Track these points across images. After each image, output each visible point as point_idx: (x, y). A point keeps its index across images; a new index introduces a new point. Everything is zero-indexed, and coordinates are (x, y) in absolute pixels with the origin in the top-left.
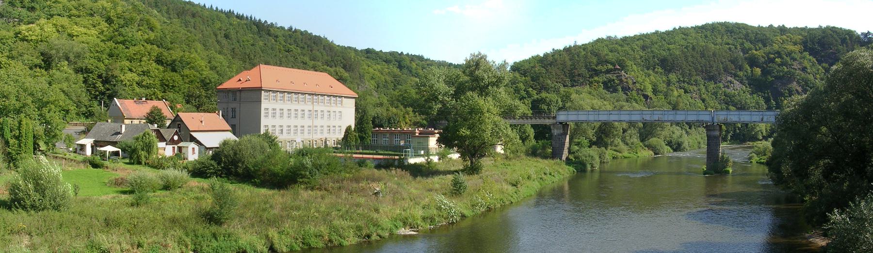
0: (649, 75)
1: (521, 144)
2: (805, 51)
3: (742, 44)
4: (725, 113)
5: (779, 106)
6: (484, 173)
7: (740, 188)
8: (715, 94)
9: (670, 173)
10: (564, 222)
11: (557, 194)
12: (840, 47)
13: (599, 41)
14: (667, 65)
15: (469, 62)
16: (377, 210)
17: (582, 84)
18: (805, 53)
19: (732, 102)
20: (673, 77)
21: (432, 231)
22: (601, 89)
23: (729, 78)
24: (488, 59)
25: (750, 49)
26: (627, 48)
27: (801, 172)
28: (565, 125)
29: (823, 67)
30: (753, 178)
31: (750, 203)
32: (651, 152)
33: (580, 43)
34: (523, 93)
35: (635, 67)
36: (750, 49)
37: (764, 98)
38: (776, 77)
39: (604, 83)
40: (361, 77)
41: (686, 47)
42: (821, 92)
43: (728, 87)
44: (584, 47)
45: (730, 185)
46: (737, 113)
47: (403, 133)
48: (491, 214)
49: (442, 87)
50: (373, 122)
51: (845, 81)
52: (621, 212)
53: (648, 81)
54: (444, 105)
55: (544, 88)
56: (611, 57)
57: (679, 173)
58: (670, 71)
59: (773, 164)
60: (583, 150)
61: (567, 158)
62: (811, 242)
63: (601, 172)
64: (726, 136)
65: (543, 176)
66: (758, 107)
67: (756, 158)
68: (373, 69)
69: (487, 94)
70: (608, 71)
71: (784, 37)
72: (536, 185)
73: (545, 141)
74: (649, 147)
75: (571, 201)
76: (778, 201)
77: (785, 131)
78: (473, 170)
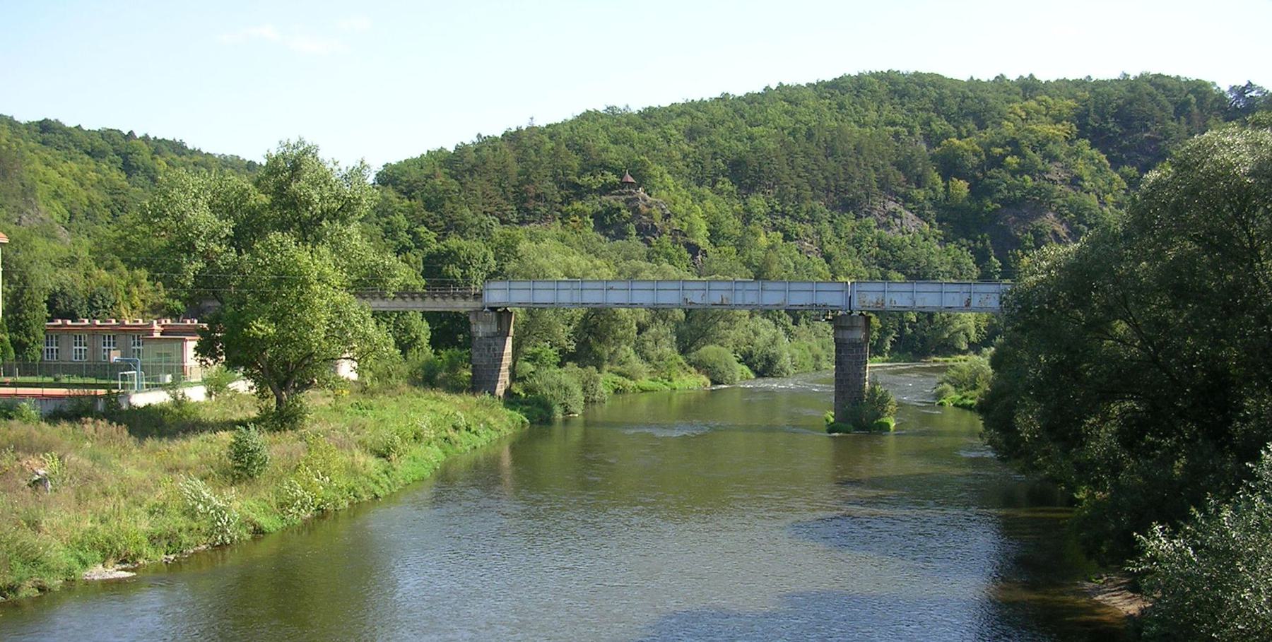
0: (702, 199)
1: (399, 358)
2: (1079, 136)
3: (927, 123)
4: (879, 287)
5: (1009, 272)
6: (310, 426)
7: (916, 467)
8: (856, 242)
9: (748, 428)
10: (502, 542)
11: (484, 475)
12: (1171, 125)
13: (588, 116)
14: (744, 175)
15: (276, 160)
16: (35, 525)
17: (544, 218)
18: (1080, 142)
19: (897, 260)
20: (758, 202)
21: (178, 563)
22: (589, 231)
23: (891, 206)
24: (320, 155)
25: (946, 135)
26: (652, 134)
27: (1064, 430)
28: (502, 315)
29: (1124, 176)
30: (947, 442)
31: (944, 501)
32: (704, 379)
33: (541, 122)
34: (405, 238)
35: (669, 179)
36: (946, 135)
37: (974, 251)
38: (1006, 203)
39: (597, 217)
40: (27, 192)
41: (793, 133)
42: (1115, 236)
43: (887, 226)
44: (552, 131)
45: (892, 459)
46: (907, 287)
47: (121, 334)
48: (326, 524)
49: (203, 218)
50: (51, 304)
51: (1177, 209)
52: (636, 519)
53: (699, 213)
54: (210, 263)
55: (455, 226)
56: (614, 154)
57: (771, 429)
58: (751, 189)
59: (995, 410)
60: (544, 371)
61: (508, 392)
62: (1099, 605)
63: (587, 424)
64: (881, 341)
65: (451, 433)
66: (957, 272)
67: (952, 396)
68: (56, 173)
69: (317, 239)
70: (606, 189)
71: (1033, 103)
72: (434, 455)
73: (455, 350)
74: (700, 366)
75: (517, 492)
76: (1009, 500)
77: (1023, 330)
78: (282, 419)
